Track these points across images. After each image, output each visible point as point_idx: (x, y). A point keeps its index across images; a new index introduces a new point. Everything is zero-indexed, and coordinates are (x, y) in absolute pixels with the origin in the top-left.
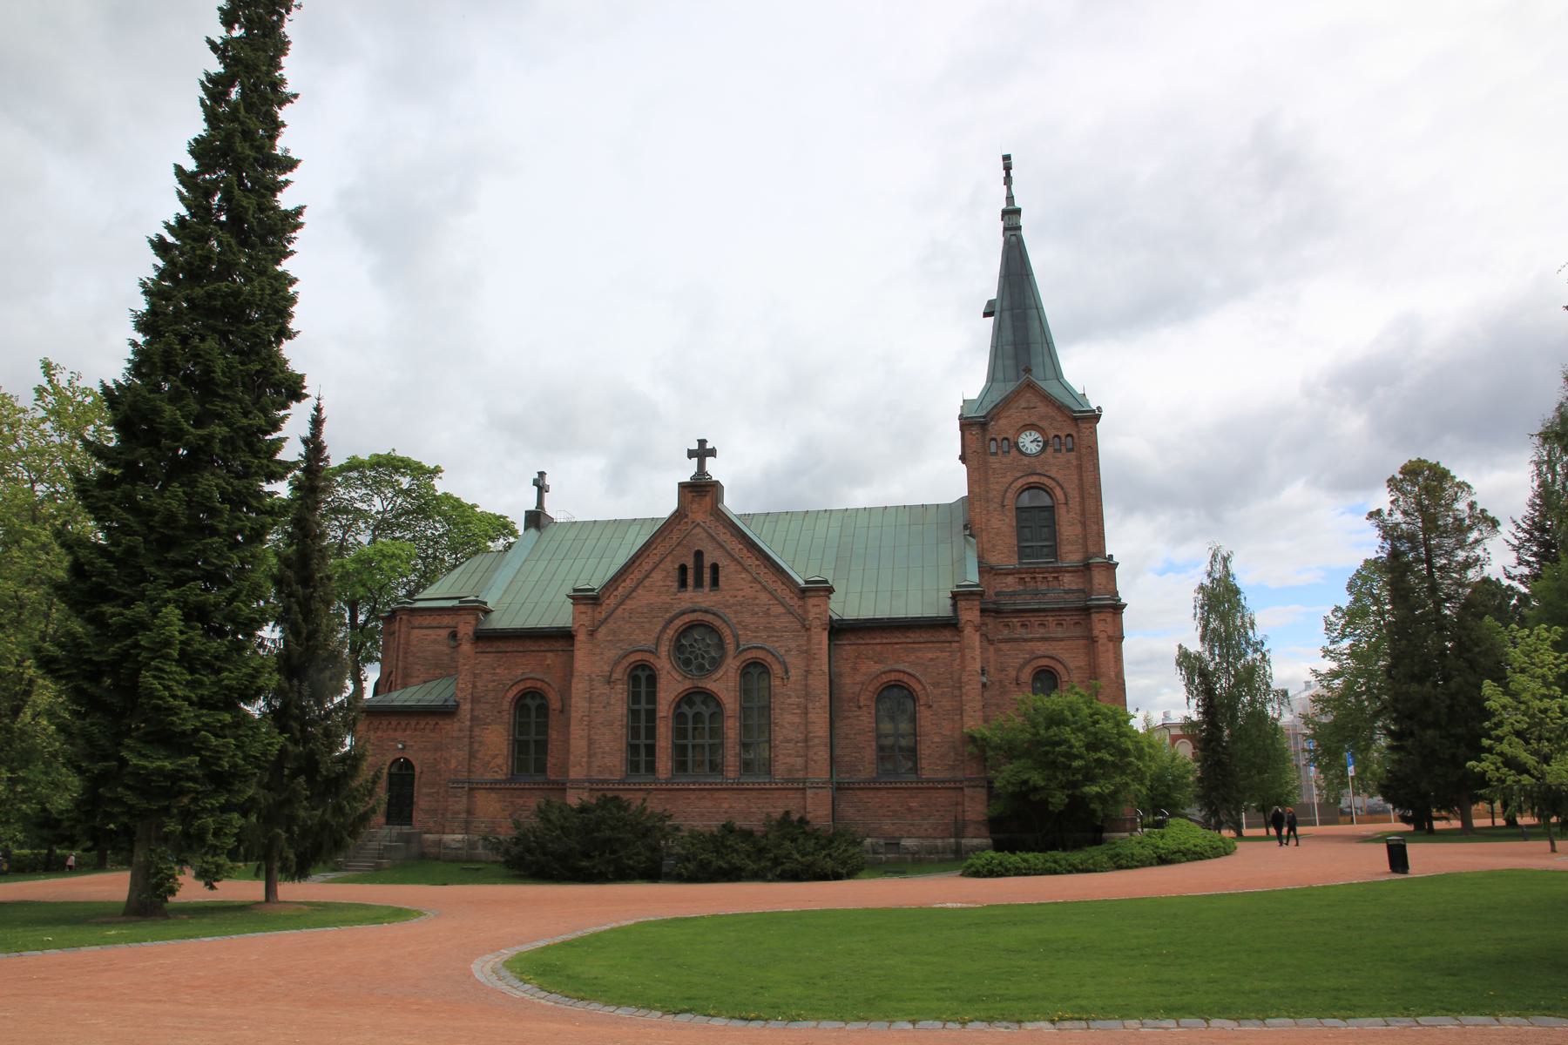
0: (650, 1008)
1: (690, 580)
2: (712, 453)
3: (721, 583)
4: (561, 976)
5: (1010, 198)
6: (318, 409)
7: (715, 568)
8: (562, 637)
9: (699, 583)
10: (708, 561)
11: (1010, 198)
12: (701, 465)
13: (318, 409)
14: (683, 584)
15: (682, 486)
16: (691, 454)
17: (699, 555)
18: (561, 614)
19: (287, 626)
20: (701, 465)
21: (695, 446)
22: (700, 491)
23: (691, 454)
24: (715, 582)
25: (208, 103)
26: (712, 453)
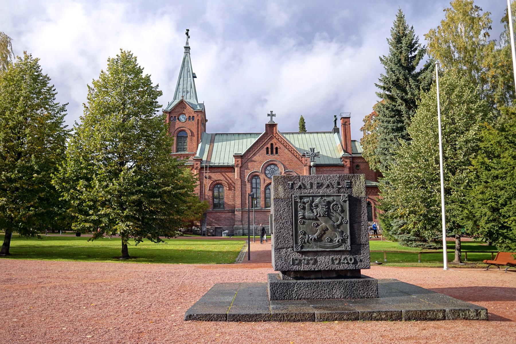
0: (421, 293)
1: (270, 152)
2: (274, 115)
3: (278, 152)
4: (80, 199)
5: (187, 43)
6: (66, 115)
7: (277, 148)
8: (231, 168)
9: (272, 153)
10: (275, 147)
11: (187, 43)
12: (272, 119)
13: (66, 115)
14: (267, 153)
15: (266, 125)
16: (269, 115)
17: (272, 144)
18: (232, 162)
19: (317, 34)
20: (272, 119)
21: (273, 113)
22: (271, 127)
23: (269, 115)
24: (277, 152)
25: (60, 199)
26: (274, 115)
